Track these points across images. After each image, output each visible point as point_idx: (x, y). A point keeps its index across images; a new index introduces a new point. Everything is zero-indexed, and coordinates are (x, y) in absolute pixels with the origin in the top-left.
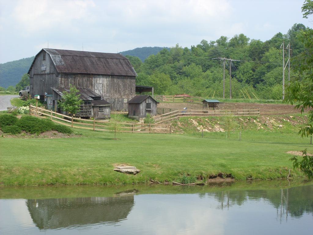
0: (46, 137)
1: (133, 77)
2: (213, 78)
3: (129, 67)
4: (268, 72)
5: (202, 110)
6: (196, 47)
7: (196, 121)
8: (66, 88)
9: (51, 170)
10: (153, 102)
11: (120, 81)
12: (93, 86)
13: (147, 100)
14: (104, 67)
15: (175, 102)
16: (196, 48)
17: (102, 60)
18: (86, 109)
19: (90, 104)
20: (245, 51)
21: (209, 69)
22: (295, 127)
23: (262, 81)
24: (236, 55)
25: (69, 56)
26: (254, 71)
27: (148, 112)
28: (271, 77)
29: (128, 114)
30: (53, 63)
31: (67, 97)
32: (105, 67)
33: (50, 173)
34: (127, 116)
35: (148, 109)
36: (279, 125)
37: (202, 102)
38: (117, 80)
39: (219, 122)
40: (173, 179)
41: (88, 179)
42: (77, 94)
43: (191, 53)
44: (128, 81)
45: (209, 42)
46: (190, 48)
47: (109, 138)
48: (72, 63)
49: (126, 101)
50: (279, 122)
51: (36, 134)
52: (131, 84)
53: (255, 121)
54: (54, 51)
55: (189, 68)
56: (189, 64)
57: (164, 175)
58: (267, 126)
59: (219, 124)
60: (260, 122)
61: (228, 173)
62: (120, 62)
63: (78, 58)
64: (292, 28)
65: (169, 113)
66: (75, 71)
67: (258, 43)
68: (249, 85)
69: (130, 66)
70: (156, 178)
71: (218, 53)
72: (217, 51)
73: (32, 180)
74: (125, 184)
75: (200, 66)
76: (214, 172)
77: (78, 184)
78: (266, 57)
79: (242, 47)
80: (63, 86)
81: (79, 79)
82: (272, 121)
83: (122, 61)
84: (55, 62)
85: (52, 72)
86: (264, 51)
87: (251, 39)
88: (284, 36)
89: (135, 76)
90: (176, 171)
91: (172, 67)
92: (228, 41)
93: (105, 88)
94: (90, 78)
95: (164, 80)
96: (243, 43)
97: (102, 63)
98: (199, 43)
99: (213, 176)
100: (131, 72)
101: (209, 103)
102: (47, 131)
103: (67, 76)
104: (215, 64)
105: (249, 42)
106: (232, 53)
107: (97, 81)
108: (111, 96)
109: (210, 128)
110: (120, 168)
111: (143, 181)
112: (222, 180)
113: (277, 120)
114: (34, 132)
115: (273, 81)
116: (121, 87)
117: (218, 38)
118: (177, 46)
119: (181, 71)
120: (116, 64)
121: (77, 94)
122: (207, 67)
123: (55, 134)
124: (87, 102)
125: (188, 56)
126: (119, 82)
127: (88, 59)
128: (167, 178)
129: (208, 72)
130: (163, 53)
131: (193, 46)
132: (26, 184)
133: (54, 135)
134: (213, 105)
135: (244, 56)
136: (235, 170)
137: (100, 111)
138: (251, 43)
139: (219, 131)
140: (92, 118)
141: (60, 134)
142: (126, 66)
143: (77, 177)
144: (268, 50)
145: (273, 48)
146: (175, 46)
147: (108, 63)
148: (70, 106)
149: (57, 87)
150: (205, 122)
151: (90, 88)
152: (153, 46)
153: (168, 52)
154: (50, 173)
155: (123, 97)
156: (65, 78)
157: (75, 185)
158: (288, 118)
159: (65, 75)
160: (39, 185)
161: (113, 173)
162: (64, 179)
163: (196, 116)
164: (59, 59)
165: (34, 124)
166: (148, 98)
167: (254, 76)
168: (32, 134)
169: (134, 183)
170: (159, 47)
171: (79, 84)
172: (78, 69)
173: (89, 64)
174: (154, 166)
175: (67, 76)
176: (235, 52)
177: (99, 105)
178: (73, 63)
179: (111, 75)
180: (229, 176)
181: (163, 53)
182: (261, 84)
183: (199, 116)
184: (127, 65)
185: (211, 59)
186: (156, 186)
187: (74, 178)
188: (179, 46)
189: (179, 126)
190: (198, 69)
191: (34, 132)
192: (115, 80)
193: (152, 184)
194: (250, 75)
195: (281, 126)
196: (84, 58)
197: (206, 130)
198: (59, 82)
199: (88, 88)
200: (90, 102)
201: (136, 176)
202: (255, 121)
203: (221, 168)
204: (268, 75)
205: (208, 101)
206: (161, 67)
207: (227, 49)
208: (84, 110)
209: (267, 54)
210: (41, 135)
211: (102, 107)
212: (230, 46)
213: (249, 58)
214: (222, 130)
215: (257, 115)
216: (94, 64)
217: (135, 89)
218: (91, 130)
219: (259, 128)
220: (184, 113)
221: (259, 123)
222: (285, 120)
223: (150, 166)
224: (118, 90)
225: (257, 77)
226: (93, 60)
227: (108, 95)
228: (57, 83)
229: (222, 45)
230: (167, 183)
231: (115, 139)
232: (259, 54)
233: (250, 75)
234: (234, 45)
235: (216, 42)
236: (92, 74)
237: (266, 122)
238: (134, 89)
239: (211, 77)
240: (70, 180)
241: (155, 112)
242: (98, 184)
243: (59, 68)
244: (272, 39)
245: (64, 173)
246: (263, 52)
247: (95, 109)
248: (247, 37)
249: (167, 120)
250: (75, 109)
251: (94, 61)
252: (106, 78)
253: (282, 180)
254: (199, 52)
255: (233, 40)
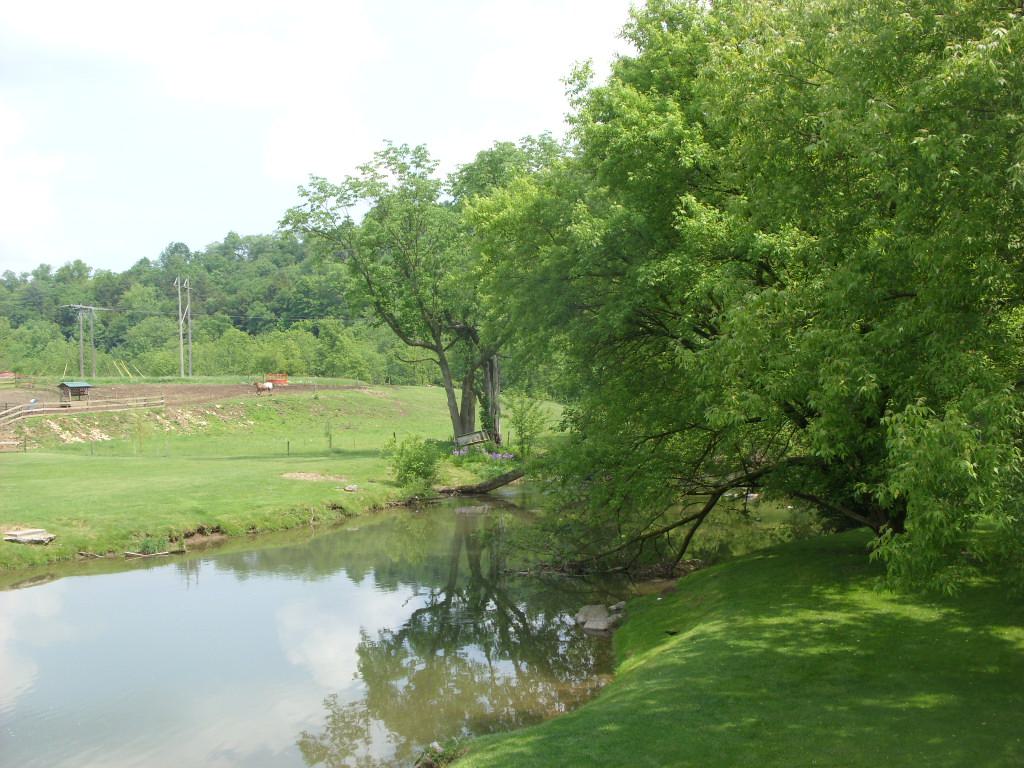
2: (33, 338)
5: (59, 403)
21: (23, 322)
23: (121, 341)
24: (72, 296)
26: (105, 324)
40: (123, 547)
45: (18, 276)
53: (158, 417)
59: (98, 426)
60: (167, 418)
65: (4, 412)
67: (109, 275)
70: (90, 548)
72: (35, 289)
74: (33, 565)
75: (6, 318)
76: (191, 528)
78: (127, 300)
79: (80, 283)
87: (95, 268)
90: (124, 532)
92: (53, 272)
96: (81, 275)
101: (72, 388)
105: (92, 273)
110: (16, 536)
112: (205, 539)
113: (196, 412)
117: (36, 267)
129: (22, 328)
134: (78, 392)
136: (223, 519)
144: (128, 289)
150: (74, 425)
158: (213, 408)
161: (6, 547)
169: (50, 562)
174: (74, 523)
180: (217, 530)
182: (120, 346)
186: (91, 563)
195: (204, 423)
197: (78, 439)
201: (48, 547)
203: (198, 517)
205: (70, 385)
212: (58, 281)
214: (106, 437)
219: (168, 429)
223: (66, 525)
225: (112, 335)
229: (43, 279)
230: (111, 555)
232: (113, 295)
234: (65, 279)
239: (28, 338)
246: (119, 292)
248: (87, 266)
253: (303, 527)
255: (62, 270)
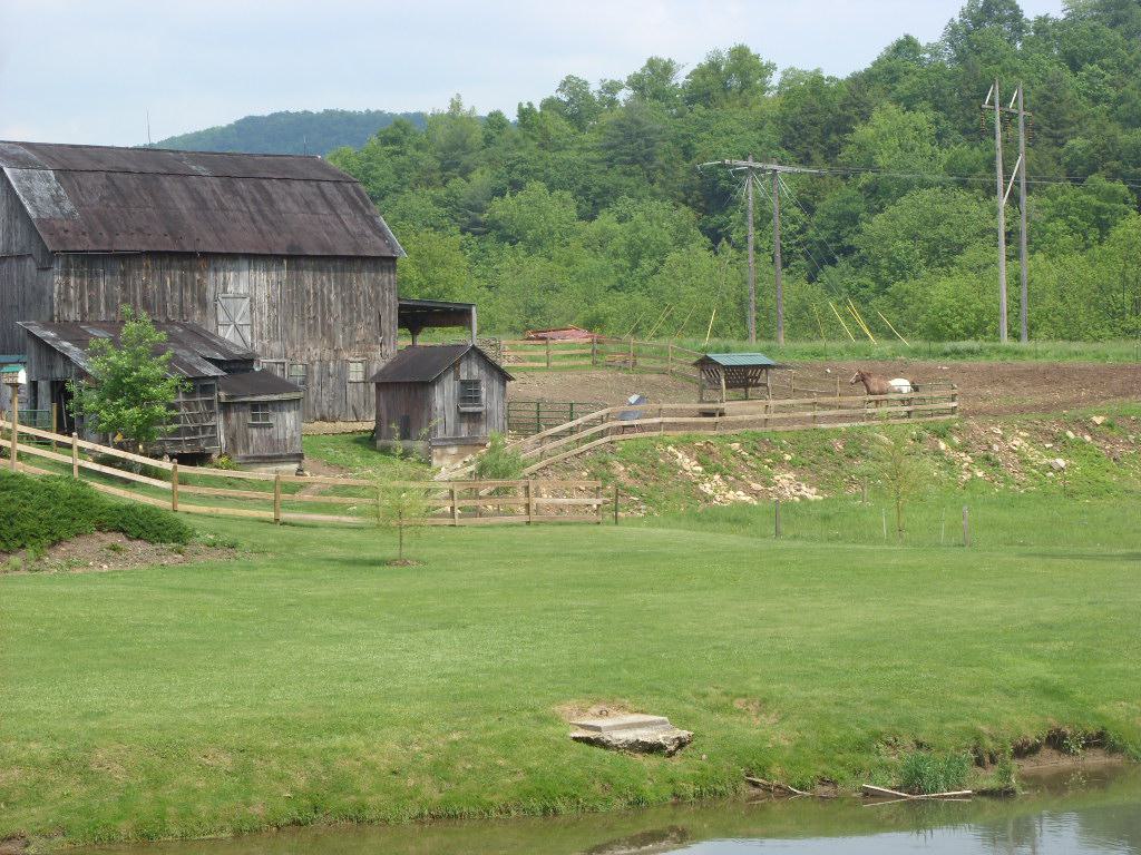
0: (77, 565)
1: (384, 263)
2: (631, 245)
3: (365, 216)
4: (873, 212)
6: (539, 110)
7: (689, 454)
8: (89, 323)
9: (278, 752)
10: (492, 375)
11: (329, 280)
12: (210, 307)
13: (463, 366)
14: (254, 221)
15: (555, 369)
16: (541, 114)
17: (241, 185)
18: (194, 418)
19: (212, 394)
20: (764, 122)
21: (605, 204)
22: (1120, 464)
25: (93, 175)
26: (808, 208)
27: (469, 421)
28: (891, 233)
29: (374, 431)
30: (22, 206)
31: (110, 364)
32: (257, 217)
33: (276, 768)
34: (370, 441)
35: (471, 409)
36: (1051, 461)
37: (695, 364)
38: (315, 280)
39: (788, 457)
41: (462, 788)
42: (157, 351)
43: (519, 135)
44: (364, 281)
45: (594, 88)
46: (512, 116)
47: (367, 555)
48: (108, 206)
49: (356, 372)
50: (1047, 446)
51: (30, 552)
52: (377, 297)
54: (22, 150)
55: (519, 204)
56: (517, 186)
57: (807, 751)
58: (996, 464)
59: (792, 465)
60: (964, 447)
61: (1092, 729)
62: (324, 196)
63: (133, 181)
64: (963, 15)
66: (124, 244)
67: (816, 84)
68: (790, 273)
69: (367, 212)
70: (776, 770)
71: (644, 133)
72: (638, 123)
73: (199, 806)
74: (638, 803)
75: (568, 195)
77: (421, 815)
78: (861, 147)
80: (73, 315)
81: (144, 279)
82: (1017, 443)
83: (329, 188)
84: (32, 201)
85: (15, 250)
86: (848, 119)
87: (782, 66)
88: (926, 51)
89: (394, 259)
91: (437, 202)
92: (680, 78)
93: (265, 319)
94: (192, 271)
95: (435, 263)
96: (746, 84)
97: (244, 200)
98: (551, 91)
99: (1027, 744)
100: (377, 238)
102: (77, 535)
103: (90, 267)
104: (631, 182)
105: (775, 80)
106: (704, 134)
107: (225, 285)
108: (290, 354)
109: (756, 486)
110: (598, 729)
111: (719, 788)
112: (1066, 762)
113: (1039, 435)
114: (19, 543)
115: (908, 254)
116: (332, 309)
117: (637, 66)
118: (456, 105)
119: (483, 217)
120: (306, 203)
121: (157, 351)
122: (598, 195)
123: (114, 548)
124: (202, 385)
125: (506, 150)
126: (322, 285)
127: (179, 186)
128: (824, 767)
129: (606, 220)
130: (394, 141)
131: (525, 106)
132: (176, 830)
133: (112, 553)
134: (744, 379)
135: (760, 143)
137: (256, 426)
138: (781, 84)
139: (797, 499)
140: (224, 460)
141: (140, 546)
142: (350, 211)
143: (411, 782)
144: (865, 118)
145: (886, 104)
146: (444, 108)
147: (271, 202)
148: (127, 408)
149: (47, 319)
150: (732, 460)
151: (196, 317)
152: (317, 107)
153: (415, 135)
154: (275, 766)
155: (345, 355)
156: (82, 276)
157: (406, 820)
158: (1084, 425)
159: (83, 263)
160: (238, 833)
162: (353, 797)
163: (686, 433)
164: (49, 189)
165: (14, 507)
166: (468, 355)
167: (811, 232)
168: (8, 553)
170: (343, 113)
171: (144, 299)
172: (139, 230)
173: (184, 206)
174: (738, 704)
175: (90, 267)
176: (718, 127)
177: (253, 395)
178: (112, 204)
179: (289, 257)
180: (1098, 741)
181: (394, 141)
182: (843, 263)
183: (701, 432)
184: (353, 204)
185: (610, 162)
186: (777, 806)
187: (397, 789)
188: (466, 107)
189: (622, 479)
190: (559, 209)
191: (19, 543)
192: (308, 279)
193: (757, 797)
194: (791, 227)
195: (1061, 462)
196: (162, 178)
197: (742, 496)
198: (55, 296)
199: (185, 318)
200: (213, 382)
201: (676, 761)
202: (943, 446)
204: (876, 224)
206: (388, 200)
207: (680, 115)
208: (185, 422)
209: (863, 132)
210: (55, 558)
211: (265, 405)
212: (691, 100)
213: (784, 152)
214: (811, 493)
215: (948, 417)
216: (208, 209)
217: (395, 317)
218: (263, 521)
220: (636, 422)
221: (963, 455)
222: (1070, 434)
224: (323, 324)
225: (823, 236)
226: (200, 188)
227: (276, 347)
228: (47, 299)
229: (655, 96)
231: (401, 562)
232: (826, 134)
233: (791, 227)
235: (629, 83)
236: (206, 255)
237: (990, 447)
238: (391, 316)
239: (619, 243)
240: (380, 797)
241: (501, 421)
242: (514, 813)
243: (52, 232)
244: (874, 64)
245: (343, 765)
246: (842, 126)
247: (233, 415)
248: (764, 61)
249: (565, 454)
250: (155, 420)
251: (205, 192)
252: (268, 270)
254: (553, 133)
255: (700, 72)
